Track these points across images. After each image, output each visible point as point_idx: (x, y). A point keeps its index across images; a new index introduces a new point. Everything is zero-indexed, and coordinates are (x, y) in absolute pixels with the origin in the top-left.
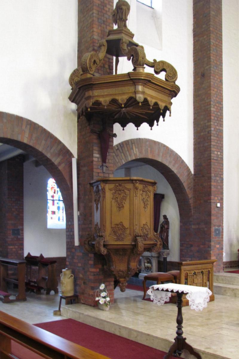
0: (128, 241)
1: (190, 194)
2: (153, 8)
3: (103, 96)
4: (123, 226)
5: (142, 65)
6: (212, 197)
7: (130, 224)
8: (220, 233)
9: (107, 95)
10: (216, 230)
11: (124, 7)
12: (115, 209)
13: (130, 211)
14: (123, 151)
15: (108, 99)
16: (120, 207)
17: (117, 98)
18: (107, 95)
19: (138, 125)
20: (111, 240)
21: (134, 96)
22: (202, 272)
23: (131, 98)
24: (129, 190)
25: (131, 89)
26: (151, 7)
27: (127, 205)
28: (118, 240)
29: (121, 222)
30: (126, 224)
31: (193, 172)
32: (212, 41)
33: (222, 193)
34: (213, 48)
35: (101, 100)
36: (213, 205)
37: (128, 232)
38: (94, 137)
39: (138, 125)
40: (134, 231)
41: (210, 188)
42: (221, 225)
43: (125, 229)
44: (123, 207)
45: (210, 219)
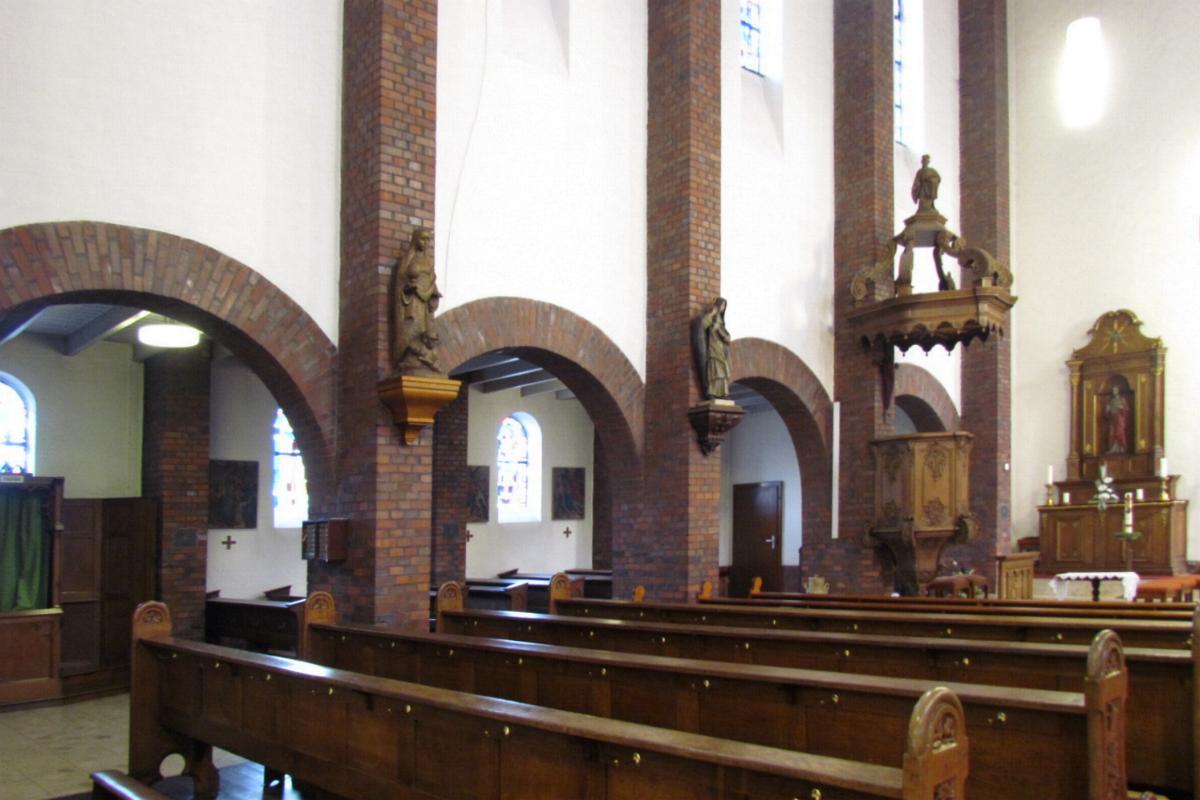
0: (947, 526)
1: (635, 420)
2: (762, 76)
3: (929, 319)
4: (940, 503)
5: (905, 244)
6: (999, 454)
7: (950, 503)
8: (1007, 512)
9: (935, 318)
10: (1004, 508)
11: (934, 180)
12: (928, 478)
13: (950, 481)
14: (63, 252)
15: (937, 323)
16: (936, 475)
17: (950, 321)
18: (935, 318)
19: (927, 348)
20: (922, 525)
21: (975, 319)
22: (1022, 572)
23: (970, 322)
24: (949, 450)
25: (971, 309)
26: (758, 74)
27: (946, 475)
28: (932, 524)
29: (938, 498)
30: (945, 501)
31: (959, 414)
32: (999, 199)
33: (1009, 447)
34: (999, 209)
35: (927, 324)
36: (999, 468)
37: (947, 511)
38: (875, 370)
39: (927, 348)
40: (956, 510)
41: (996, 440)
42: (1008, 501)
43: (943, 507)
44: (940, 475)
45: (996, 491)
